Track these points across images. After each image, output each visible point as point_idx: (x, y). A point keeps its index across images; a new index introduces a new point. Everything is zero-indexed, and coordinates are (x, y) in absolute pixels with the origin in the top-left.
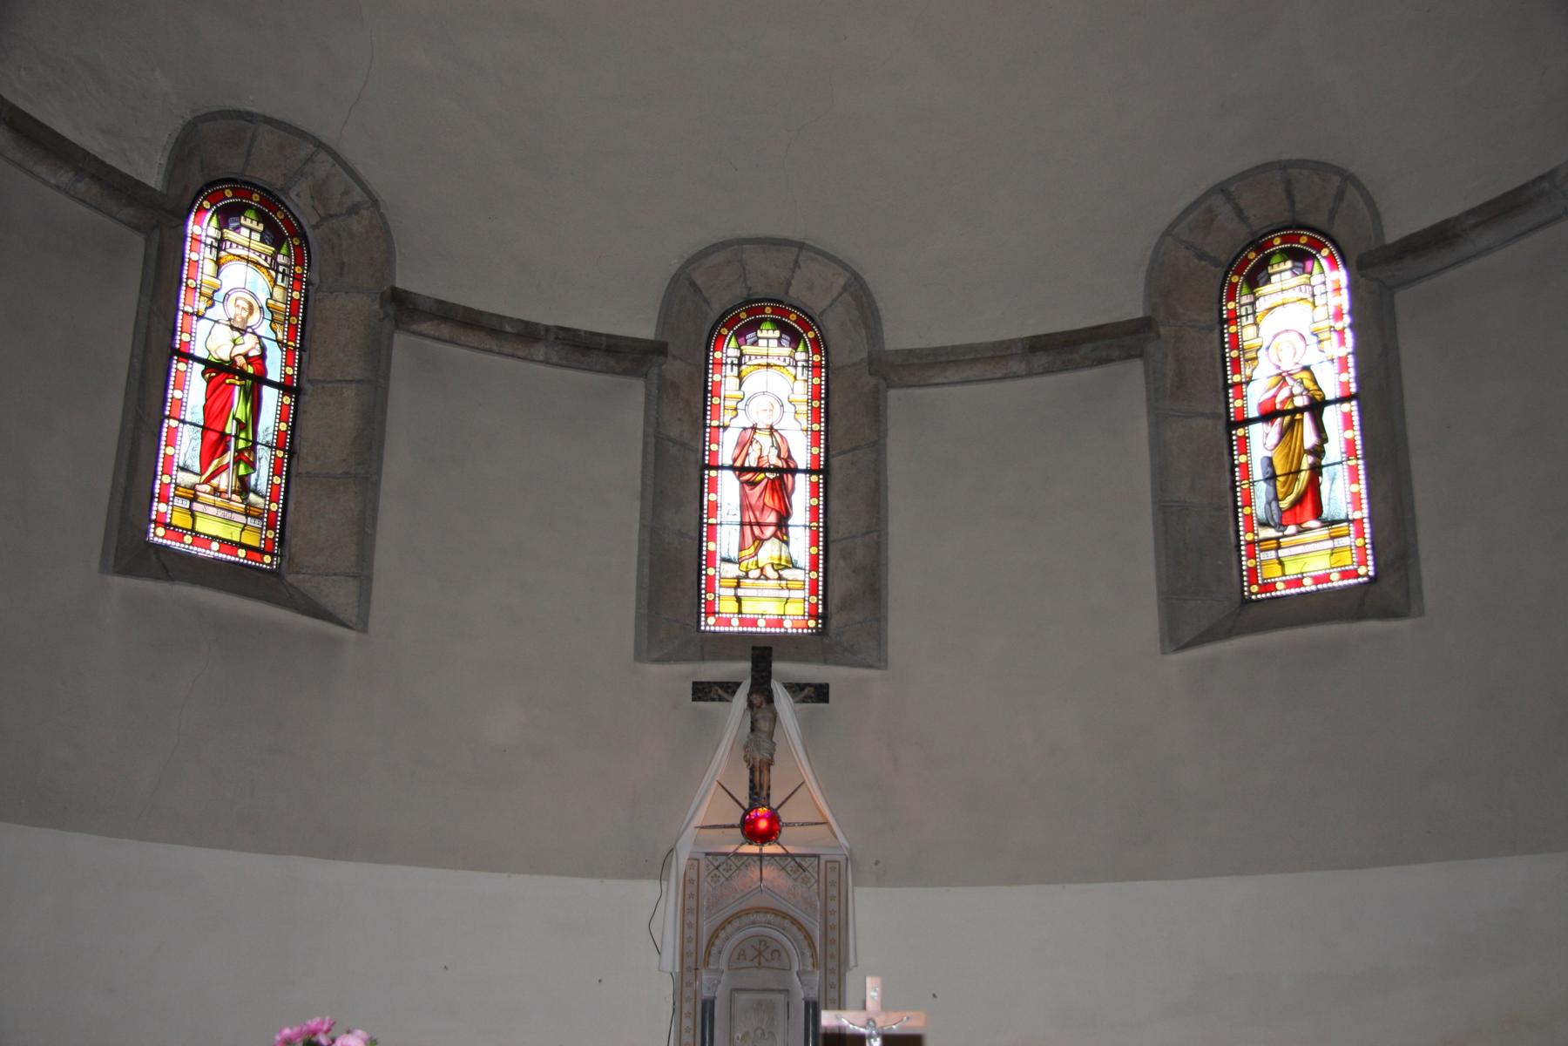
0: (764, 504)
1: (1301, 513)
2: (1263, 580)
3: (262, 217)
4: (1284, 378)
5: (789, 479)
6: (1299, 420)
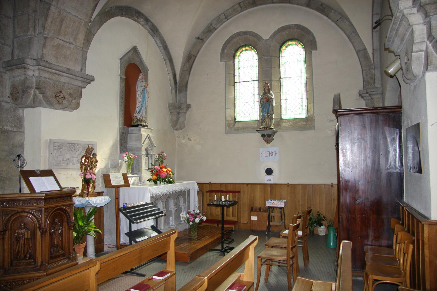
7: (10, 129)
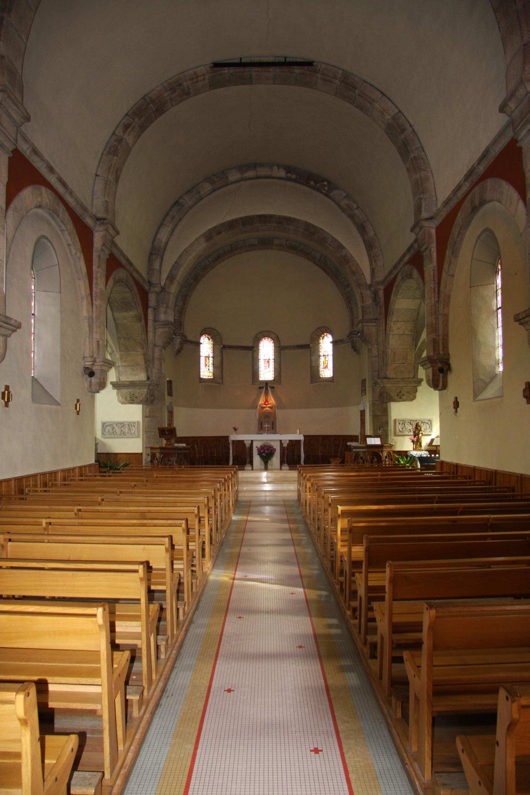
7: (380, 414)
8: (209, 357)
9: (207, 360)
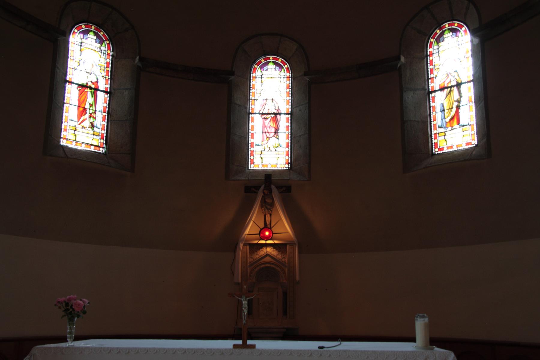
0: (270, 126)
1: (453, 123)
2: (440, 147)
3: (96, 34)
4: (448, 75)
5: (278, 116)
6: (453, 90)
8: (96, 89)
9: (89, 95)
